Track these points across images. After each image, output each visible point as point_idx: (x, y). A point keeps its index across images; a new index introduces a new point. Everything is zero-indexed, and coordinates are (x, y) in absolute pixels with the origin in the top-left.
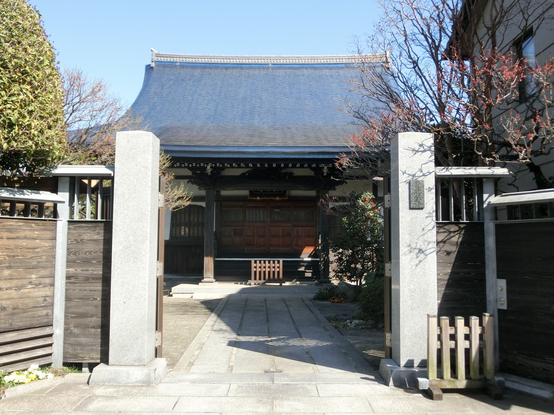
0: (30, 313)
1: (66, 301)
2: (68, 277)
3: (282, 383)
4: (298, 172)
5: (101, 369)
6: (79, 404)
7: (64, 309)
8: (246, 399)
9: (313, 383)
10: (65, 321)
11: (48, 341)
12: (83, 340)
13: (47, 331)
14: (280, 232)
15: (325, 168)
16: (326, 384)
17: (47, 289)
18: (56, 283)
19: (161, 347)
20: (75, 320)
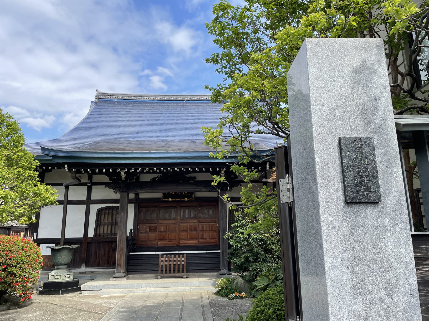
14: (188, 227)
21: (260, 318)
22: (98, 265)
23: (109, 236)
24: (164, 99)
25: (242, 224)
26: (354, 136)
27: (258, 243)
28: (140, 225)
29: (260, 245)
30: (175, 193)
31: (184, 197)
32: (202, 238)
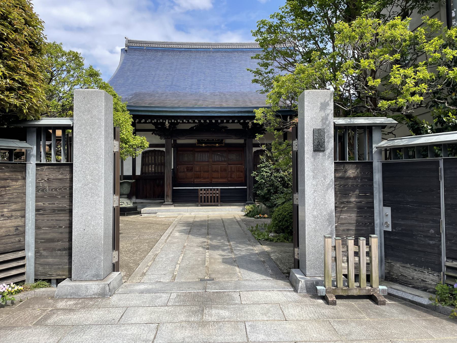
0: (4, 241)
1: (35, 229)
2: (37, 210)
3: (213, 291)
4: (231, 126)
5: (65, 283)
6: (40, 318)
7: (34, 236)
8: (182, 308)
9: (237, 291)
10: (35, 246)
11: (21, 263)
12: (50, 260)
13: (20, 254)
14: (219, 168)
15: (250, 123)
16: (248, 291)
17: (18, 220)
18: (27, 215)
19: (118, 262)
20: (44, 244)
21: (279, 217)
22: (145, 197)
23: (153, 175)
24: (191, 47)
25: (266, 165)
26: (319, 128)
27: (277, 180)
28: (179, 166)
29: (279, 181)
30: (208, 140)
31: (216, 143)
32: (231, 177)
